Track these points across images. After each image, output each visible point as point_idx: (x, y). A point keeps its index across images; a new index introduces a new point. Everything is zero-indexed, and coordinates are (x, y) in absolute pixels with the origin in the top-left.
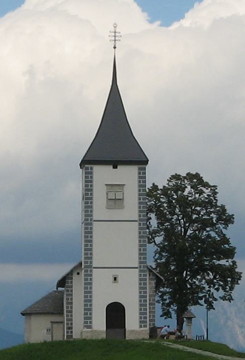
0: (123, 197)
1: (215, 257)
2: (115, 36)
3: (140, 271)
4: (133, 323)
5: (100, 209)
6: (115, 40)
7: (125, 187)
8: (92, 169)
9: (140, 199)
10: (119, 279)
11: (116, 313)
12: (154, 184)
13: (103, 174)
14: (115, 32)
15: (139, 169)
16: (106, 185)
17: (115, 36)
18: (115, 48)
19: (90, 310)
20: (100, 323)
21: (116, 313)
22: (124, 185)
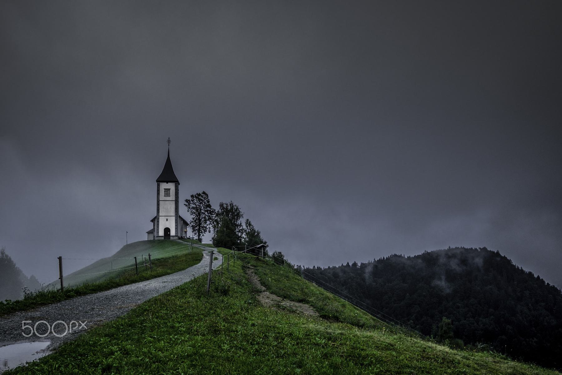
0: (158, 186)
1: (239, 241)
2: (169, 142)
3: (176, 217)
4: (173, 233)
5: (162, 197)
6: (169, 140)
7: (170, 190)
8: (159, 184)
9: (175, 230)
10: (168, 220)
11: (167, 230)
12: (147, 233)
13: (164, 186)
14: (169, 140)
15: (175, 184)
16: (164, 189)
17: (169, 142)
18: (169, 145)
19: (159, 227)
20: (161, 233)
21: (167, 230)
22: (170, 189)
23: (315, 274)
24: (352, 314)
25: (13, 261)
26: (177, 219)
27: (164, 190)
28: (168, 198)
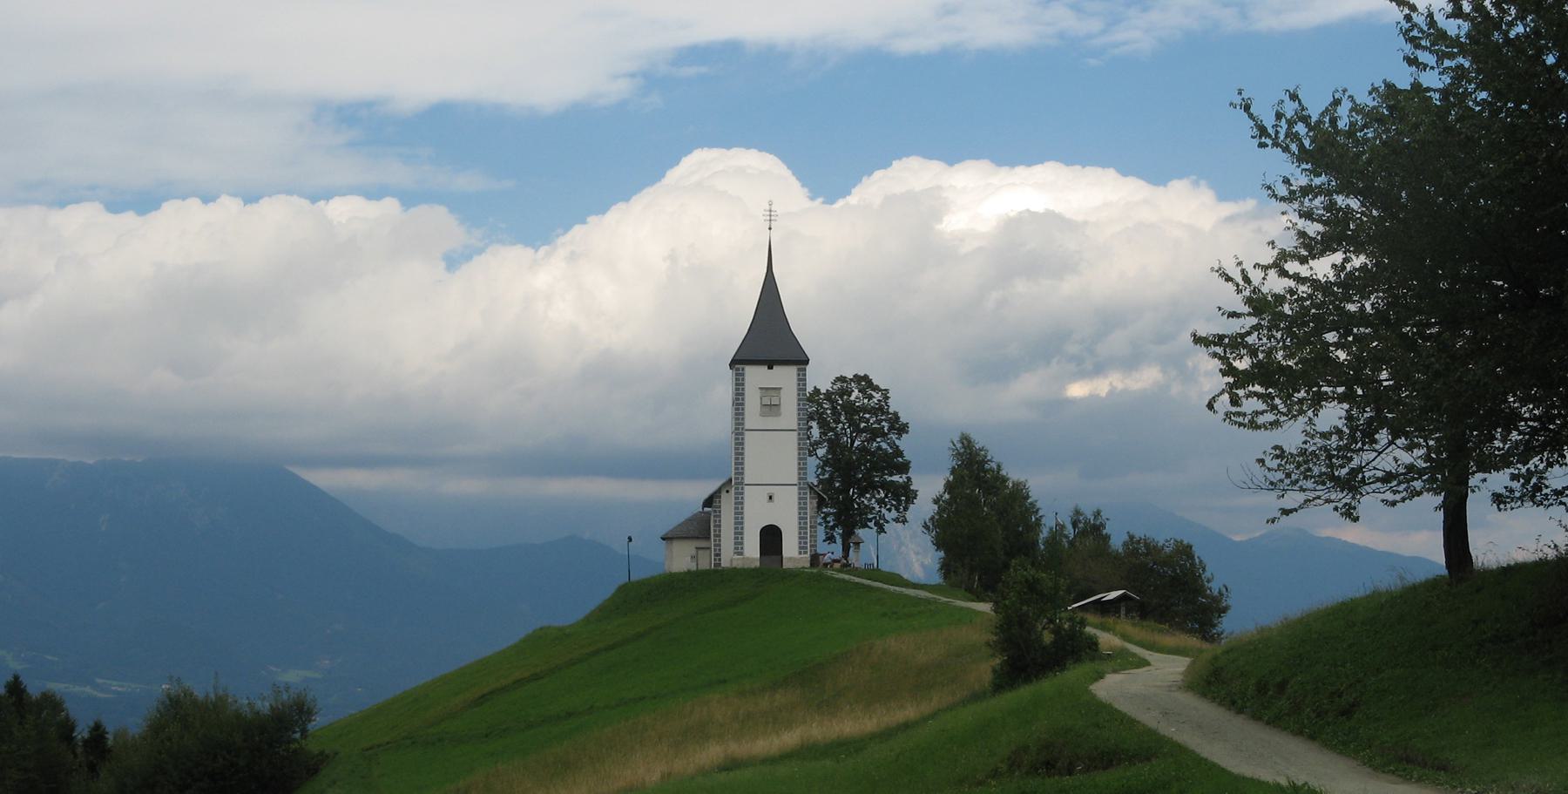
2: (770, 215)
3: (800, 489)
4: (791, 549)
6: (770, 220)
7: (782, 391)
10: (775, 498)
11: (771, 537)
13: (757, 376)
14: (770, 211)
15: (799, 370)
16: (760, 388)
17: (770, 215)
20: (752, 549)
21: (771, 537)
22: (781, 388)
23: (1508, 500)
24: (1289, 686)
25: (1508, 565)
26: (805, 504)
27: (758, 394)
28: (771, 422)
